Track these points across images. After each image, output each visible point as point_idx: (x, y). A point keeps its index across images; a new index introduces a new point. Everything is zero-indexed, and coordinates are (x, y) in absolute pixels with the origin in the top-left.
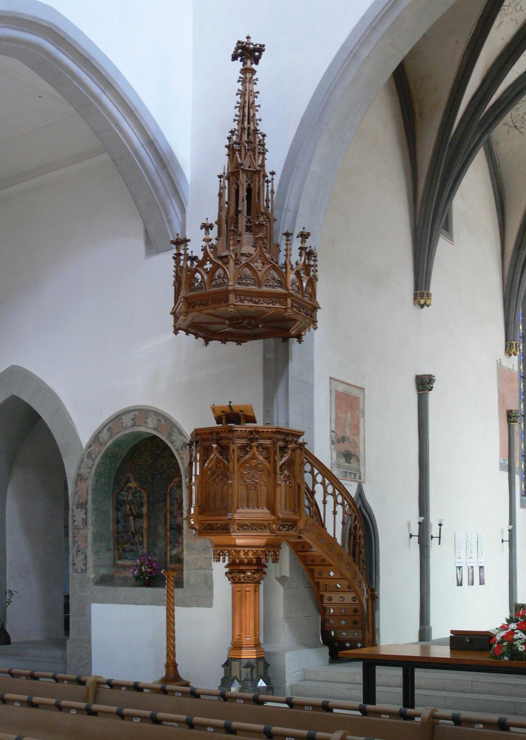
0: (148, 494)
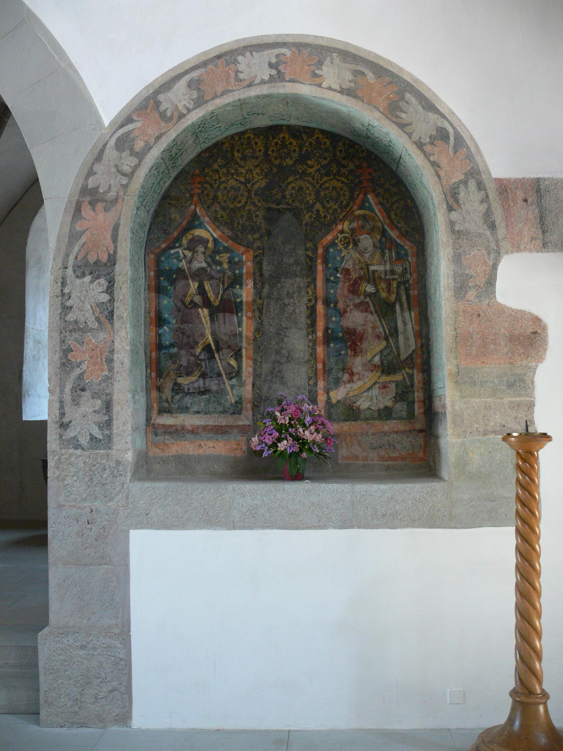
0: (255, 257)
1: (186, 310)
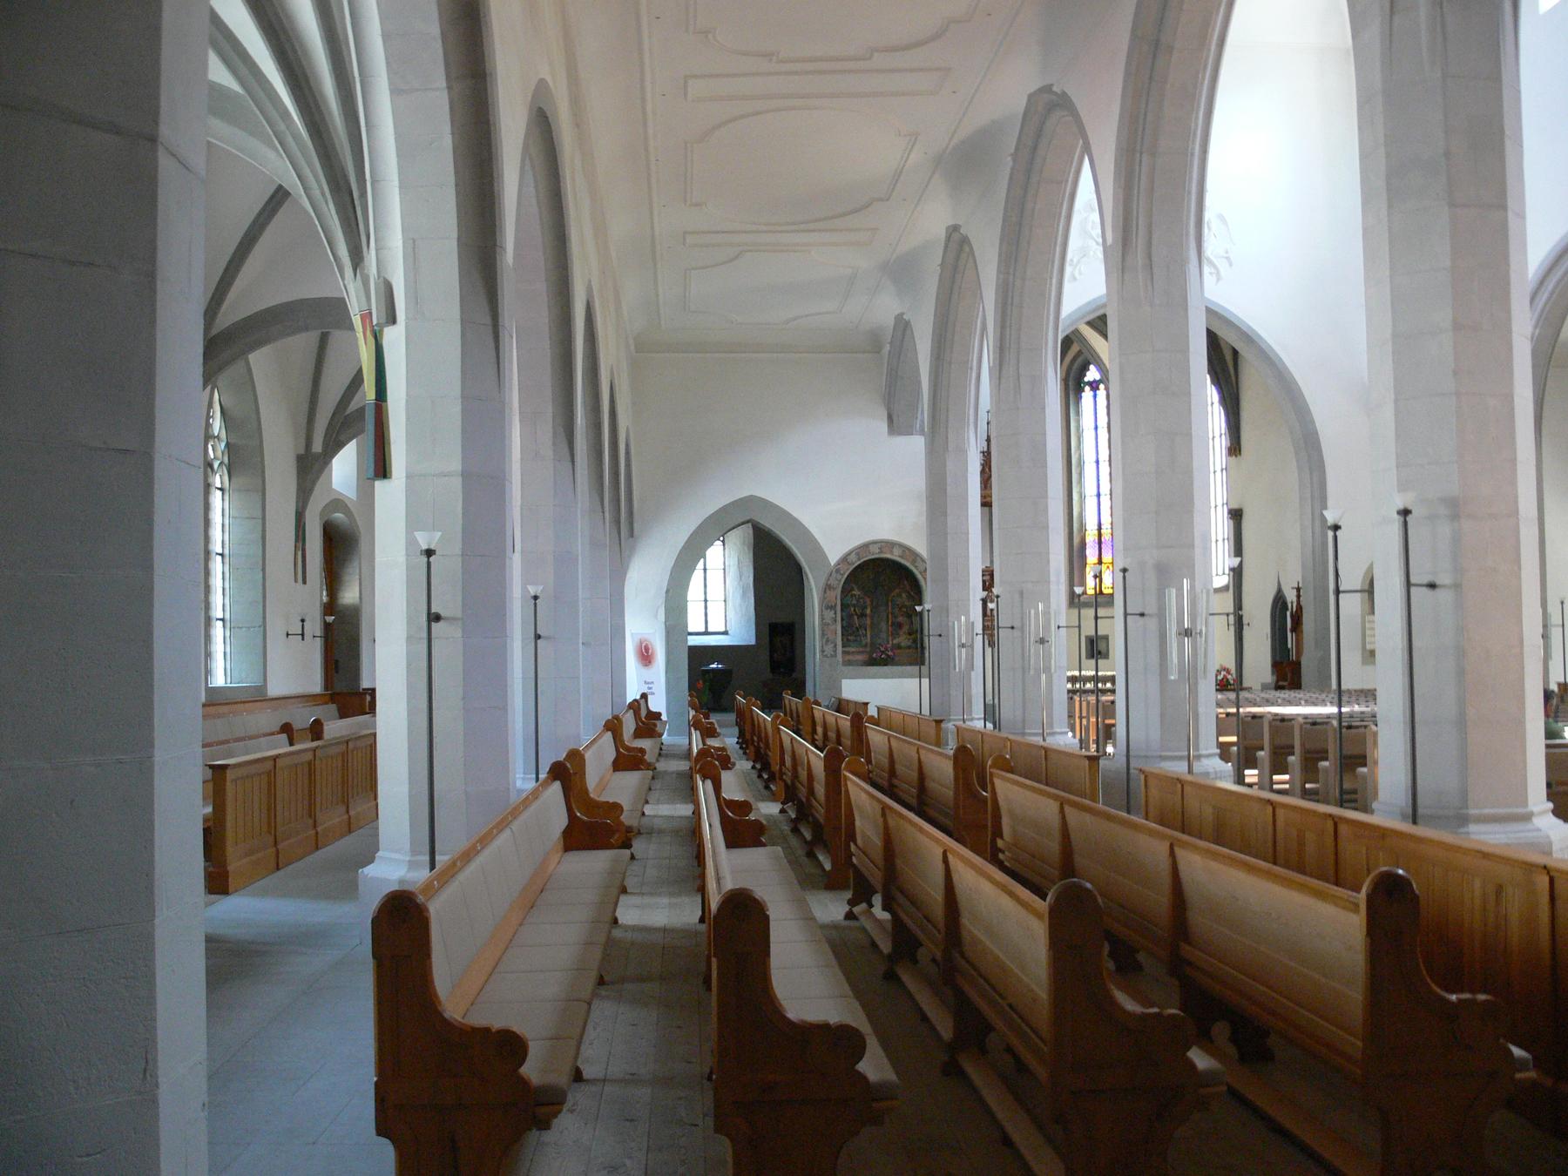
1: (850, 616)
